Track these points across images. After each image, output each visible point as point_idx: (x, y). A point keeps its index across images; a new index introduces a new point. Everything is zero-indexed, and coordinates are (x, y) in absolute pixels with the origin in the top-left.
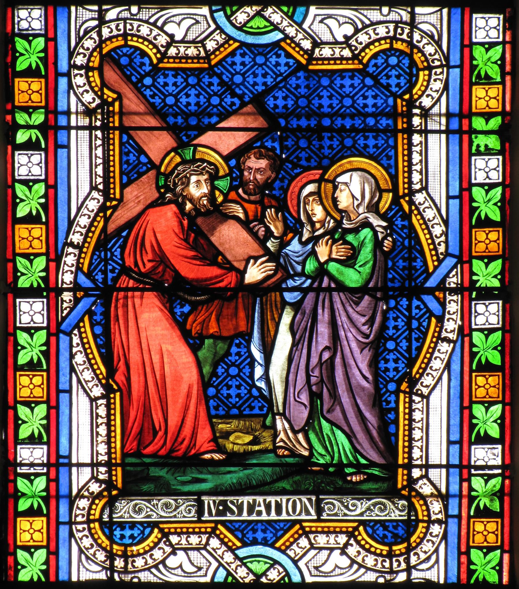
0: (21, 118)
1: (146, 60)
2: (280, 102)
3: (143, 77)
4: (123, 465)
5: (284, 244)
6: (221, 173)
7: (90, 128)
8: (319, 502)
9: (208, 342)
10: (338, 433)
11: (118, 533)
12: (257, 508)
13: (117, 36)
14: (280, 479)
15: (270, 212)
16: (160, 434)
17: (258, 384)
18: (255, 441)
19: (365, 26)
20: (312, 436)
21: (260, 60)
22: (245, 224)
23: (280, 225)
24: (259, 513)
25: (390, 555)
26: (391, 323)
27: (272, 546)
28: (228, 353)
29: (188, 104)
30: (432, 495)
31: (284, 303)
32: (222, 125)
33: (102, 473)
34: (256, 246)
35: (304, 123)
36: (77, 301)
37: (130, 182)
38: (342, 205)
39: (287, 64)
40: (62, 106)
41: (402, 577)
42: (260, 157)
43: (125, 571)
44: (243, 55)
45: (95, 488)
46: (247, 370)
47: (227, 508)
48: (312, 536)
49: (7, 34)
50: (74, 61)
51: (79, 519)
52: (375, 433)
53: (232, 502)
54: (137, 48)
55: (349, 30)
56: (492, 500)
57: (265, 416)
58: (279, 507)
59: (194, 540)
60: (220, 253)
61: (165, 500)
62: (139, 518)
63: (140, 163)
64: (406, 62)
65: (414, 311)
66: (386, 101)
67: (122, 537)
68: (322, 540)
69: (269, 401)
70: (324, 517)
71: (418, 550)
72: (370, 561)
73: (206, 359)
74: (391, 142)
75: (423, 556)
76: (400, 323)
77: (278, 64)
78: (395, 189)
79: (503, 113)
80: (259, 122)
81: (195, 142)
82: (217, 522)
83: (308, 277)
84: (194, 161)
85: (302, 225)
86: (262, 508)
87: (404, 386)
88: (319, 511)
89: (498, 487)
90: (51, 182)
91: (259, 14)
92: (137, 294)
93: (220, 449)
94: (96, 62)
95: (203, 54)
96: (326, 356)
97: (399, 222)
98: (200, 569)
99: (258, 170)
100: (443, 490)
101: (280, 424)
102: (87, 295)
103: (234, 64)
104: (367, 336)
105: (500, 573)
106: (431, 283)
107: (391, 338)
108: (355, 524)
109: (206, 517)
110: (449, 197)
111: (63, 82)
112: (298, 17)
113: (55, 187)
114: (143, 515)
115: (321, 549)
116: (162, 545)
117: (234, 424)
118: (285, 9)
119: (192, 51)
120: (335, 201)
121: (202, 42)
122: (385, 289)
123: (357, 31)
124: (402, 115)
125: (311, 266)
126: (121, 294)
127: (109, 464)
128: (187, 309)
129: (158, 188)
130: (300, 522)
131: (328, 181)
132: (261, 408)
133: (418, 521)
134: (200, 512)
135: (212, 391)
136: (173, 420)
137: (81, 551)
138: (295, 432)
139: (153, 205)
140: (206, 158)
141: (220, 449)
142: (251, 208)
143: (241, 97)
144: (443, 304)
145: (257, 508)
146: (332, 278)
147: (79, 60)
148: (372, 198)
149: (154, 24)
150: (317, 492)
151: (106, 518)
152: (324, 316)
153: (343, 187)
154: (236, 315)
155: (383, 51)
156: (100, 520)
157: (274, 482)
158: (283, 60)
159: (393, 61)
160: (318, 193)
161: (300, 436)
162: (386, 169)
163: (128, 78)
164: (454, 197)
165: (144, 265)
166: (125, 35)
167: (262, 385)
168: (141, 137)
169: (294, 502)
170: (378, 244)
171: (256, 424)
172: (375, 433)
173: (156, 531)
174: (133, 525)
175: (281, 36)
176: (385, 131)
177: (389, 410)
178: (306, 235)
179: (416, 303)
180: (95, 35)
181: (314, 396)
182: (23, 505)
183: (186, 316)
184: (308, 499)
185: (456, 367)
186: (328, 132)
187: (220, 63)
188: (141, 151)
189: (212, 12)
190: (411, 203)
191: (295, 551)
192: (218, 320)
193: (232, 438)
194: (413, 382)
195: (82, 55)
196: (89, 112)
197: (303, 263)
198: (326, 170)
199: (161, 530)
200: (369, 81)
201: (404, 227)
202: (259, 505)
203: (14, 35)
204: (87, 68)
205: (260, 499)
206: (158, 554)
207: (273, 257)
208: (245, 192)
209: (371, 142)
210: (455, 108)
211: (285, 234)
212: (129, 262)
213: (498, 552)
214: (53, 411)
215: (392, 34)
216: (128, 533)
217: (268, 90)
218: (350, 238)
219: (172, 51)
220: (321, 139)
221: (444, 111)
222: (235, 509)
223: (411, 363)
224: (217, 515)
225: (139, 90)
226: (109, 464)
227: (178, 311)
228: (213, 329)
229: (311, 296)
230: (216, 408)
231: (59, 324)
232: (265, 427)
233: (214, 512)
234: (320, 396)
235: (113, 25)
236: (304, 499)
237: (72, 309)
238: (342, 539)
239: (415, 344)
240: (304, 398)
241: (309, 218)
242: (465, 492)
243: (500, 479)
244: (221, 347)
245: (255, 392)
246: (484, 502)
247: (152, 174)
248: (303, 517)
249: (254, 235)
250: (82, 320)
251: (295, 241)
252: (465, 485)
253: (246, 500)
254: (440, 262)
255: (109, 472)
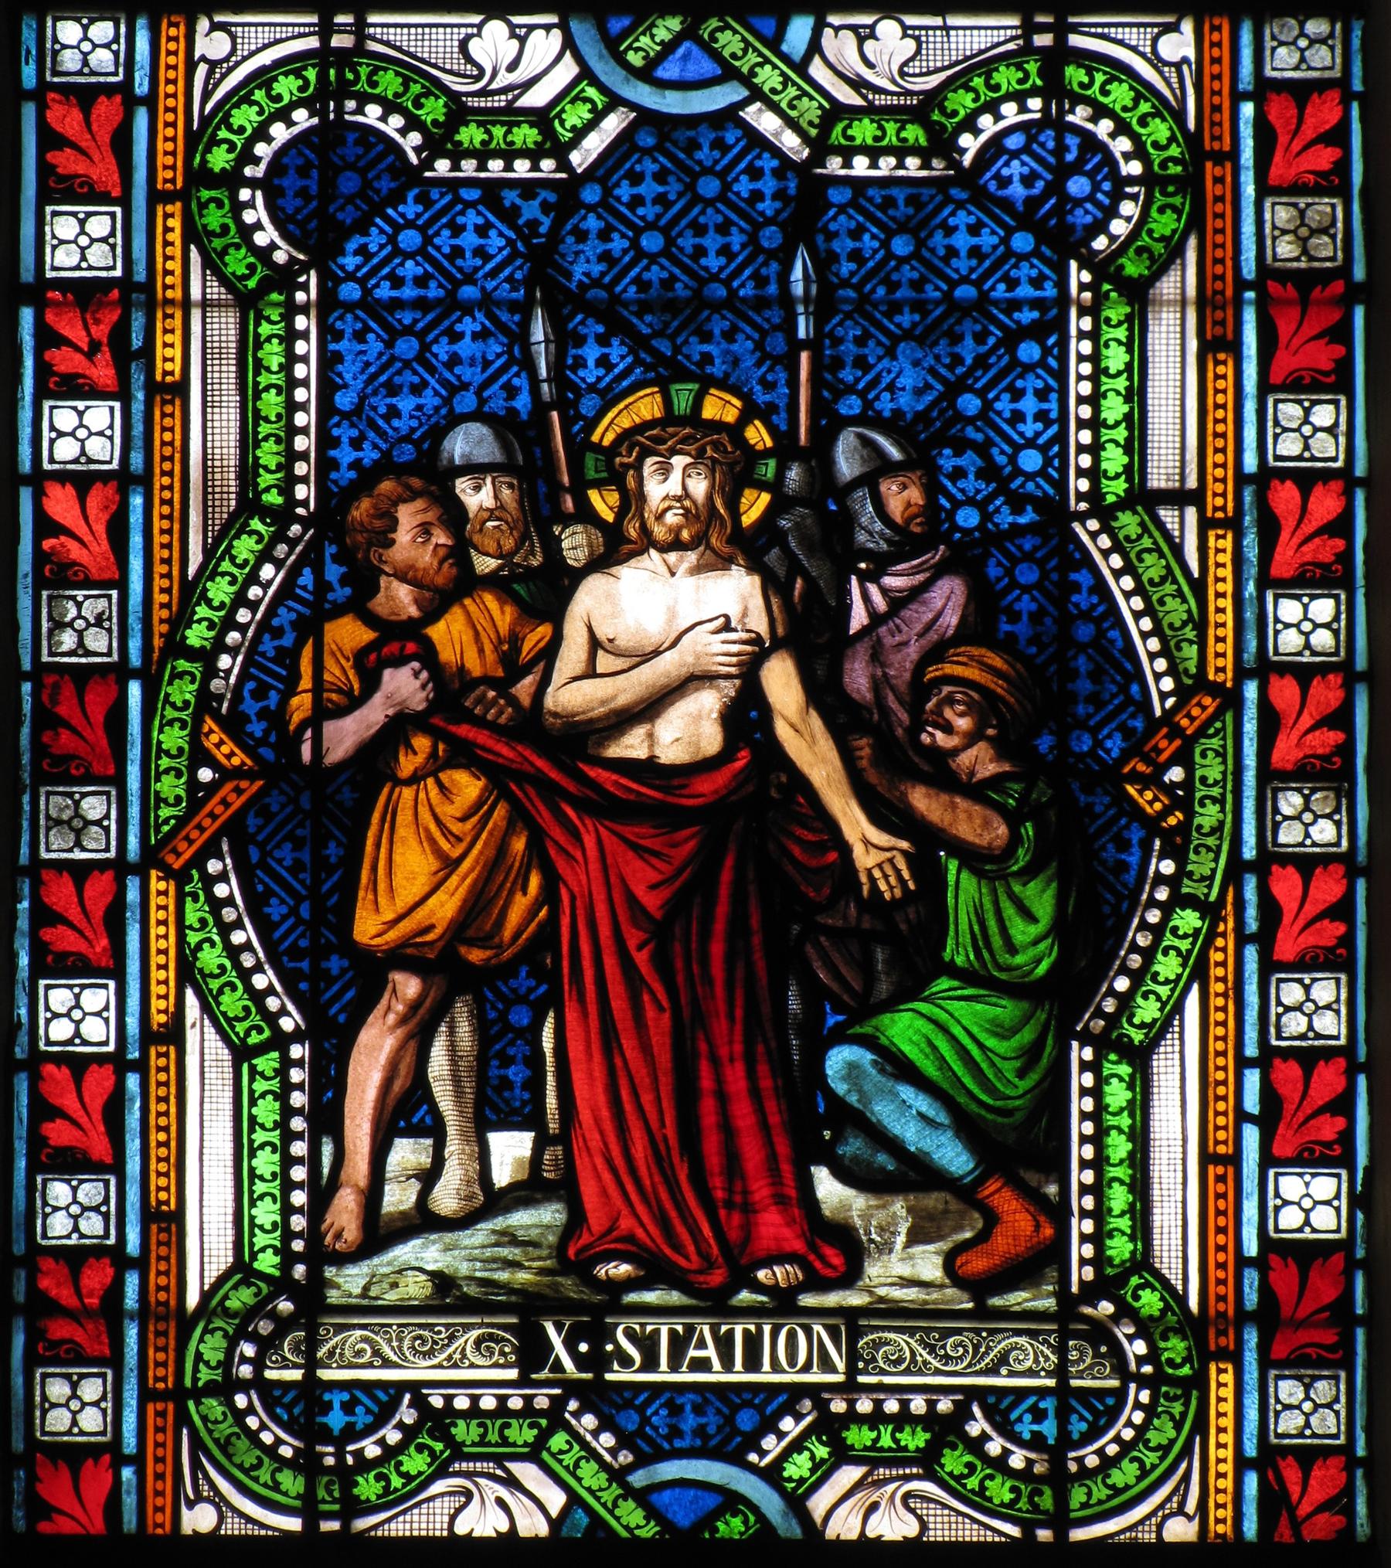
12: (693, 1353)
24: (702, 1365)
50: (204, 161)
53: (630, 1334)
58: (753, 1343)
86: (711, 1352)
130: (813, 1391)
145: (693, 1353)
169: (792, 1337)
184: (826, 1327)
186: (551, 228)
195: (225, 146)
202: (701, 1344)
222: (636, 1356)
248: (815, 1377)
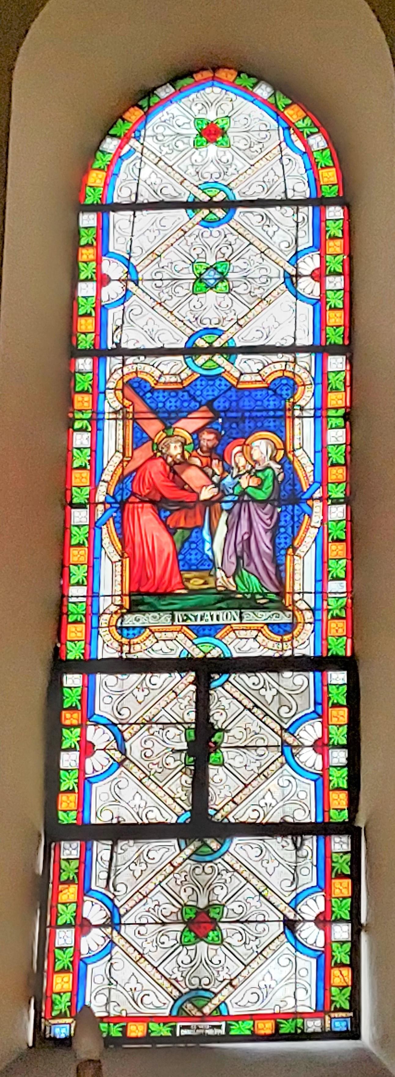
0: (78, 415)
1: (148, 385)
2: (222, 405)
3: (145, 393)
4: (130, 595)
5: (222, 479)
6: (188, 442)
7: (116, 419)
8: (241, 613)
9: (179, 531)
10: (252, 577)
11: (125, 632)
13: (132, 373)
14: (219, 601)
15: (215, 462)
16: (151, 581)
17: (206, 552)
18: (205, 583)
19: (269, 364)
20: (237, 579)
21: (211, 383)
22: (201, 469)
23: (221, 469)
25: (282, 641)
26: (282, 519)
27: (214, 637)
28: (190, 536)
29: (171, 407)
30: (306, 609)
31: (222, 510)
32: (190, 416)
33: (118, 600)
34: (208, 480)
35: (234, 415)
36: (106, 510)
37: (136, 449)
38: (255, 457)
39: (226, 385)
40: (100, 409)
41: (288, 653)
42: (210, 433)
43: (129, 652)
44: (201, 380)
45: (113, 609)
46: (201, 546)
47: (188, 618)
48: (237, 632)
49: (71, 372)
51: (104, 625)
52: (273, 577)
54: (142, 379)
55: (260, 366)
56: (340, 610)
57: (211, 570)
58: (218, 617)
59: (170, 635)
60: (186, 484)
61: (152, 614)
62: (137, 624)
63: (142, 438)
64: (292, 382)
65: (296, 512)
66: (280, 402)
67: (128, 634)
68: (242, 634)
69: (213, 561)
70: (243, 622)
71: (298, 638)
72: (270, 644)
73: (178, 540)
74: (283, 424)
75: (301, 642)
76: (288, 518)
77: (220, 385)
78: (285, 449)
79: (346, 407)
80: (211, 415)
81: (174, 426)
82: (182, 626)
83: (236, 495)
84: (173, 436)
85: (233, 468)
86: (209, 618)
87: (290, 551)
88: (241, 618)
89: (344, 604)
90: (94, 448)
91: (210, 359)
92: (140, 505)
93: (186, 588)
94: (120, 386)
95: (179, 381)
96: (246, 537)
97: (287, 466)
98: (172, 650)
99: (208, 440)
100: (312, 606)
101: (220, 573)
102: (111, 507)
103: (196, 385)
104: (268, 525)
105: (346, 649)
106: (306, 496)
107: (282, 527)
108: (262, 625)
109: (176, 623)
110: (315, 452)
111: (102, 396)
112: (231, 360)
113: (95, 451)
114: (141, 621)
115: (241, 639)
116: (151, 638)
117: (194, 574)
118: (225, 356)
119: (173, 379)
120: (251, 456)
121: (179, 374)
122: (279, 499)
123: (264, 367)
124: (289, 410)
125: (237, 490)
126: (131, 506)
127: (122, 595)
128: (168, 513)
129: (153, 451)
131: (248, 445)
132: (209, 565)
133: (298, 623)
134: (173, 619)
135: (180, 557)
136: (159, 571)
137: (104, 642)
138: (227, 577)
139: (151, 459)
140: (180, 434)
141: (186, 588)
142: (204, 460)
143: (200, 402)
144: (311, 508)
146: (249, 495)
147: (111, 385)
148: (272, 452)
149: (153, 366)
150: (240, 609)
151: (119, 625)
152: (244, 516)
153: (256, 448)
154: (195, 515)
155: (279, 377)
156: (116, 626)
157: (215, 604)
158: (223, 382)
159: (284, 382)
160: (242, 451)
161: (231, 580)
162: (281, 439)
163: (138, 393)
164: (319, 452)
165: (144, 491)
166: (136, 372)
167: (210, 553)
168: (144, 424)
170: (275, 478)
171: (205, 574)
172: (273, 577)
173: (148, 630)
174: (134, 628)
175: (223, 370)
176: (280, 417)
177: (281, 565)
178: (235, 473)
179: (296, 507)
180: (120, 371)
181: (238, 558)
182: (71, 619)
183: (167, 517)
185: (319, 541)
187: (188, 385)
188: (143, 431)
189: (185, 359)
190: (294, 455)
191: (227, 640)
192: (185, 519)
193: (191, 581)
194: (295, 550)
196: (116, 412)
197: (233, 489)
198: (246, 439)
199: (151, 630)
200: (271, 392)
201: (290, 468)
203: (75, 372)
204: (115, 389)
205: (207, 613)
206: (148, 643)
207: (217, 485)
208: (201, 451)
209: (272, 424)
210: (319, 405)
211: (223, 473)
212: (136, 490)
213: (345, 638)
214: (91, 569)
215: (283, 368)
216: (131, 632)
217: (214, 400)
218: (259, 474)
219: (163, 380)
220: (244, 422)
221: (312, 407)
223: (294, 539)
224: (183, 621)
225: (144, 400)
226: (122, 595)
227: (163, 515)
228: (182, 524)
229: (238, 505)
230: (183, 566)
231: (96, 523)
232: (210, 575)
233: (181, 620)
234: (242, 558)
235: (130, 367)
236: (233, 612)
237: (103, 515)
238: (255, 633)
239: (296, 529)
240: (234, 559)
241: (237, 465)
242: (325, 607)
243: (345, 599)
244: (187, 533)
245: (205, 557)
246: (336, 612)
247: (150, 442)
248: (233, 621)
249: (206, 474)
250: (108, 520)
251: (229, 477)
252: (325, 603)
253: (199, 614)
254: (310, 485)
255: (122, 600)
